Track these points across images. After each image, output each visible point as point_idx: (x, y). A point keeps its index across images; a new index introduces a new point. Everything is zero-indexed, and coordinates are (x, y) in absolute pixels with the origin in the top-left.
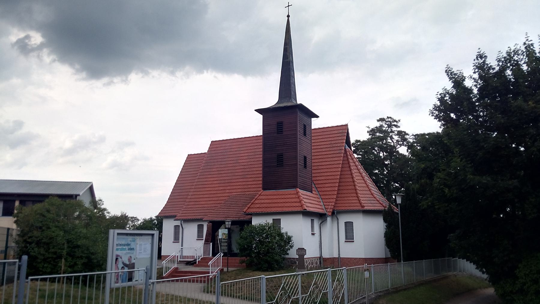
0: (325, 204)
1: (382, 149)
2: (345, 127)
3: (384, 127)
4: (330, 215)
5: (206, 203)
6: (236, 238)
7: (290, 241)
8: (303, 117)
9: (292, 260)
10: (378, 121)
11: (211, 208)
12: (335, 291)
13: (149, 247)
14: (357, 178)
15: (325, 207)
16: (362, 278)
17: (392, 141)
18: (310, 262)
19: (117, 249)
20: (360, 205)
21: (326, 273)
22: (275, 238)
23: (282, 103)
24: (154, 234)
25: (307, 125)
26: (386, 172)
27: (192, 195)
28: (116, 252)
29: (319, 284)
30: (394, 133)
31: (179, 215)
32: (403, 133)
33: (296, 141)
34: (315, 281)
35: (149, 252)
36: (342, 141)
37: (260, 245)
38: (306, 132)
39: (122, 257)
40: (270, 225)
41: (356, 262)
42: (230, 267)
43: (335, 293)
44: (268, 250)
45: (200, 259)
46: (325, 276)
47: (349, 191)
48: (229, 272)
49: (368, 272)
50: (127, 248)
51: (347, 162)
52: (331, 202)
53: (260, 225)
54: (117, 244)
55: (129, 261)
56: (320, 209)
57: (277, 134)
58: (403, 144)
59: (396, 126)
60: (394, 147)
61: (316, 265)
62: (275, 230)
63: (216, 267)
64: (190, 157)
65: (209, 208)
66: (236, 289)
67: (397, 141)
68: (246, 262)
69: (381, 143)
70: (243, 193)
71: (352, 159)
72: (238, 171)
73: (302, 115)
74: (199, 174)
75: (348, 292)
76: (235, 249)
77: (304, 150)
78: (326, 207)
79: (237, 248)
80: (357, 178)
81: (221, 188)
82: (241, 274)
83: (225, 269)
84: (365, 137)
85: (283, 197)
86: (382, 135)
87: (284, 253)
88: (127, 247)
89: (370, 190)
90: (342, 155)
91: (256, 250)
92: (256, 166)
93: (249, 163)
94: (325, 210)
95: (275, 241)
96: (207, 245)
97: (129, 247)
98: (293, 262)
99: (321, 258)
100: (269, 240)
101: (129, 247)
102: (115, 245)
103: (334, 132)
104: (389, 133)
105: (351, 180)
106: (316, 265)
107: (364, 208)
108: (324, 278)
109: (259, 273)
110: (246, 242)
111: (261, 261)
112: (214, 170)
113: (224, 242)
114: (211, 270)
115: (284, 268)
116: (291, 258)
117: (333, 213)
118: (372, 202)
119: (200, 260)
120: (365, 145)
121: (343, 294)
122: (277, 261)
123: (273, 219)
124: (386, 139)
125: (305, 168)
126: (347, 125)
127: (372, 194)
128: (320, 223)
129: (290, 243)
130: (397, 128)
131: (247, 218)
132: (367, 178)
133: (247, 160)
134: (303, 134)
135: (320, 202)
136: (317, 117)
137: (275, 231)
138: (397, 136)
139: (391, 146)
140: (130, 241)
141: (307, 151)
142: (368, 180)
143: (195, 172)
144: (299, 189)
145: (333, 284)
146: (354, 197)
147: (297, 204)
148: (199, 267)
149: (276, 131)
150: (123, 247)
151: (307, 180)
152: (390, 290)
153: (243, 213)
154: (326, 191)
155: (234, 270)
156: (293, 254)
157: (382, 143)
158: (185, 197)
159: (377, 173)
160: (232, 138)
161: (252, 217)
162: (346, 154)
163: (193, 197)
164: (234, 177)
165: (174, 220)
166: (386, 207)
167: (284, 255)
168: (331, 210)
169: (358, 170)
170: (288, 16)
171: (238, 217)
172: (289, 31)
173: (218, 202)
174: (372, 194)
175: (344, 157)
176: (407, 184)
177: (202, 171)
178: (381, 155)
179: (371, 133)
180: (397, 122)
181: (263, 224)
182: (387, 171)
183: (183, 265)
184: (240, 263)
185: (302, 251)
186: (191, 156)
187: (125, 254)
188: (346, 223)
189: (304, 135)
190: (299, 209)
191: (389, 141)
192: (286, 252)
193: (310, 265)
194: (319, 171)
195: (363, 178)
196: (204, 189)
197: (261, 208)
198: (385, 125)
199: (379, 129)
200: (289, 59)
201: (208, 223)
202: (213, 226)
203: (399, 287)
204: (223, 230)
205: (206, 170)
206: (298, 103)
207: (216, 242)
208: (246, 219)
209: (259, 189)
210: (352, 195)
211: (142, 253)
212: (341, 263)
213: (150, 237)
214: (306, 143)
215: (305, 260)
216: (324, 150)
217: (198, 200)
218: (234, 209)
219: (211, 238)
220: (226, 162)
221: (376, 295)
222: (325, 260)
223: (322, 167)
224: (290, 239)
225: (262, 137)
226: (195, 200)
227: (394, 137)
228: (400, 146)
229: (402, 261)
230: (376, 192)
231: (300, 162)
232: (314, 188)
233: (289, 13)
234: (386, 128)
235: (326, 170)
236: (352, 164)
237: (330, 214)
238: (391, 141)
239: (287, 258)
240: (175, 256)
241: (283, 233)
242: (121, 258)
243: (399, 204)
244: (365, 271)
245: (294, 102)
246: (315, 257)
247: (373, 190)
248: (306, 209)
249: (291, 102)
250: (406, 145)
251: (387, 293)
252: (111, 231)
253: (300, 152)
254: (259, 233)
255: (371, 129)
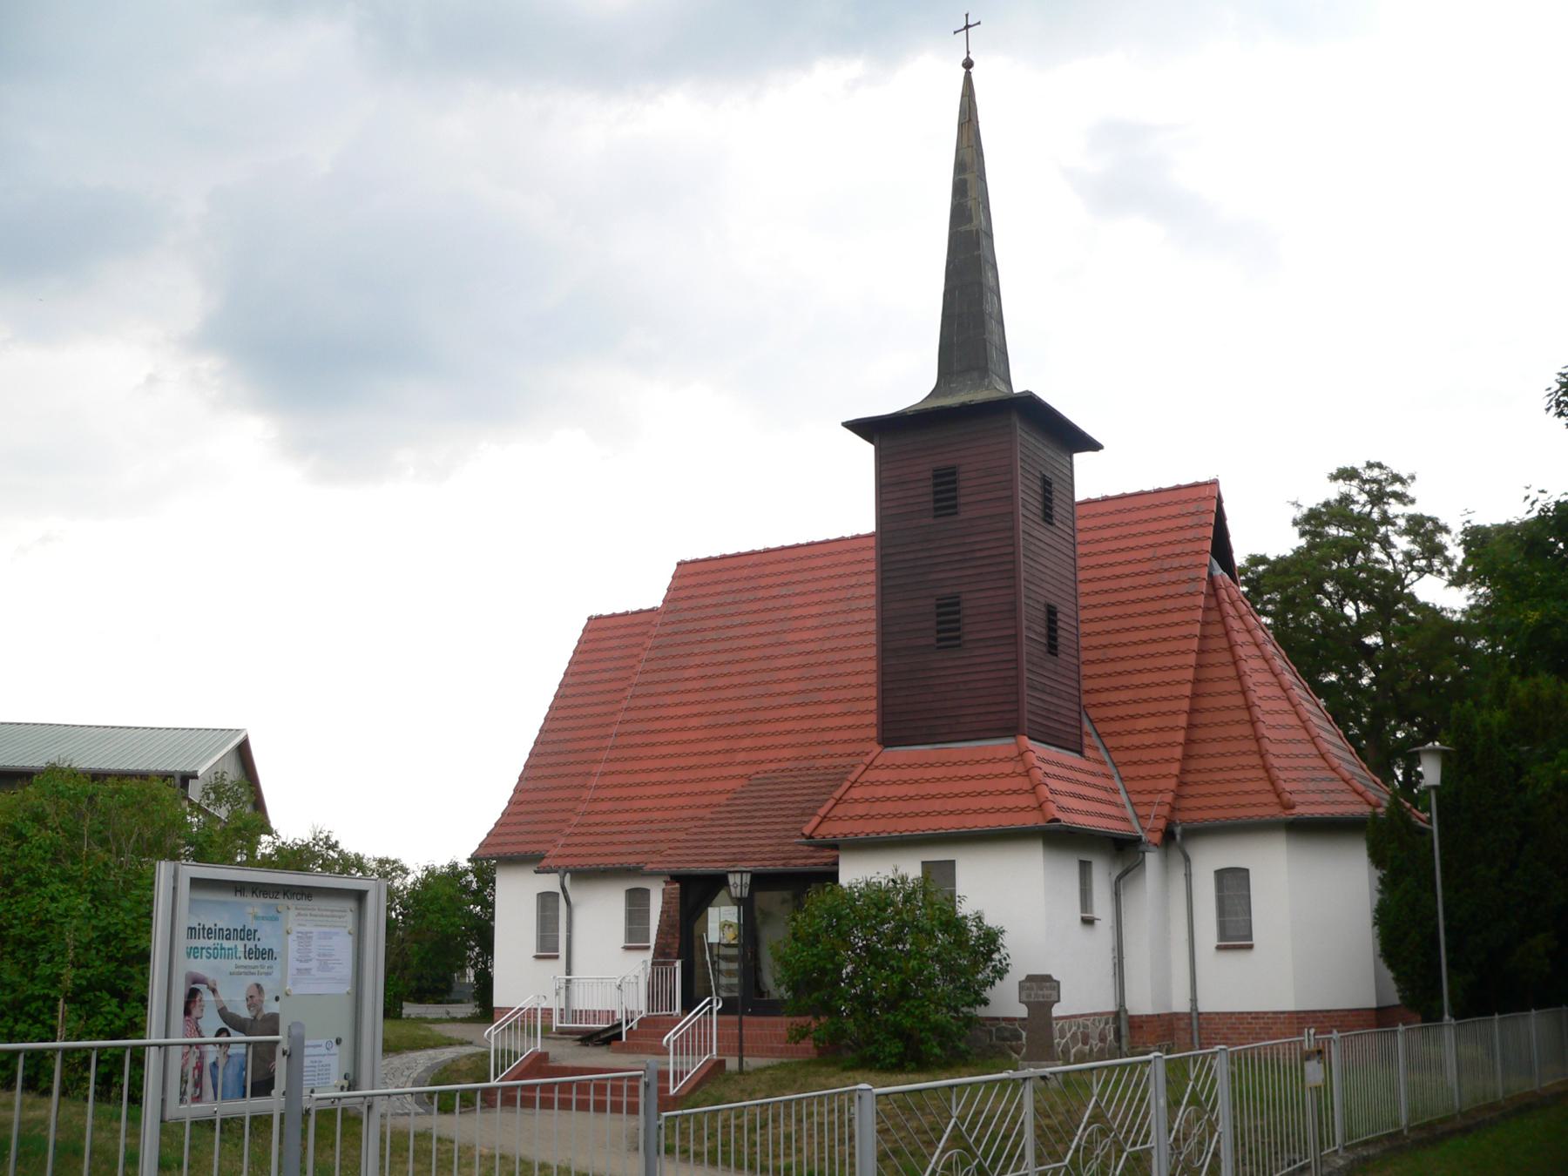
0: (1136, 798)
1: (1351, 587)
2: (1207, 492)
3: (1357, 502)
4: (1156, 845)
5: (658, 803)
6: (775, 937)
7: (993, 952)
8: (1040, 446)
9: (1003, 1024)
10: (1334, 478)
11: (679, 825)
12: (1178, 1147)
13: (342, 946)
14: (1261, 692)
15: (1135, 812)
16: (1297, 1092)
17: (1390, 556)
18: (1074, 1035)
19: (193, 952)
20: (1276, 800)
21: (1142, 1073)
22: (930, 935)
23: (951, 393)
24: (366, 892)
25: (1057, 480)
26: (1371, 679)
27: (604, 774)
28: (187, 966)
29: (1114, 1117)
30: (1394, 524)
31: (555, 852)
32: (1429, 525)
33: (1013, 545)
34: (1094, 1107)
35: (346, 969)
36: (1196, 547)
37: (872, 968)
38: (1051, 509)
39: (218, 989)
40: (909, 886)
41: (1261, 1028)
42: (748, 1056)
43: (1181, 1153)
44: (904, 984)
45: (634, 1024)
46: (1137, 1085)
47: (1233, 747)
48: (749, 1073)
49: (1319, 1063)
50: (241, 949)
51: (1218, 630)
52: (1161, 792)
53: (867, 884)
54: (191, 929)
55: (249, 1007)
56: (1116, 818)
57: (935, 517)
58: (1429, 569)
59: (1400, 497)
60: (1398, 578)
61: (1099, 1044)
62: (932, 904)
63: (693, 1054)
64: (598, 630)
65: (669, 826)
66: (776, 1143)
67: (1409, 557)
68: (816, 1034)
69: (1346, 564)
70: (805, 764)
71: (1241, 617)
72: (782, 675)
73: (1033, 441)
74: (629, 692)
75: (1236, 1145)
76: (773, 983)
77: (1048, 579)
78: (1142, 811)
79: (775, 980)
80: (1261, 692)
81: (718, 746)
82: (795, 1081)
83: (732, 1063)
84: (1283, 542)
85: (964, 771)
86: (1348, 534)
87: (969, 995)
88: (240, 945)
89: (1313, 740)
90: (1201, 600)
91: (854, 987)
92: (854, 655)
93: (827, 645)
94: (1135, 823)
95: (930, 950)
96: (664, 968)
97: (250, 944)
98: (1007, 1034)
99: (1122, 1015)
100: (908, 946)
101: (250, 944)
102: (181, 932)
103: (1164, 512)
104: (1374, 526)
105: (1239, 700)
106: (1099, 1044)
107: (1294, 811)
108: (1135, 1092)
109: (865, 1076)
110: (813, 955)
111: (875, 1031)
112: (687, 674)
113: (728, 959)
114: (675, 1063)
115: (969, 1058)
116: (997, 1019)
117: (1168, 837)
118: (1323, 786)
119: (635, 1028)
120: (1286, 571)
121: (1216, 1155)
122: (941, 1032)
123: (923, 863)
124: (1367, 550)
125: (1050, 652)
126: (1215, 483)
127: (1323, 756)
128: (1114, 878)
129: (994, 956)
130: (1405, 504)
131: (817, 861)
132: (1299, 692)
133: (820, 634)
134: (1042, 516)
135: (1116, 791)
136: (1094, 446)
137: (932, 907)
138: (1406, 538)
139: (1386, 572)
140: (256, 917)
141: (1058, 584)
142: (1307, 701)
143: (614, 686)
144: (1030, 738)
145: (1171, 1121)
146: (1253, 767)
147: (1023, 801)
148: (629, 1053)
149: (931, 505)
150: (220, 942)
151: (1061, 703)
152: (1405, 1132)
153: (804, 840)
154: (1138, 747)
155: (769, 1067)
156: (1005, 1001)
157: (1352, 562)
158: (577, 781)
159: (1332, 682)
160: (759, 547)
161: (838, 856)
162: (1217, 600)
163: (608, 780)
164: (766, 702)
165: (536, 872)
166: (1379, 806)
167: (969, 1005)
168: (1161, 824)
169: (1267, 661)
170: (968, 64)
171: (784, 859)
172: (970, 120)
173: (706, 800)
174: (1323, 756)
175: (1207, 609)
176: (1461, 707)
177: (643, 678)
178: (1349, 610)
179: (1307, 527)
180: (1403, 482)
181: (884, 882)
182: (1372, 675)
183: (570, 1043)
184: (791, 1038)
185: (1041, 988)
186: (600, 623)
187: (231, 974)
188: (1221, 875)
189: (1046, 521)
190: (1032, 820)
191: (1378, 554)
192: (977, 994)
193: (1075, 1044)
194: (1110, 668)
195: (1285, 691)
196: (648, 751)
197: (873, 817)
198: (1359, 494)
199: (1338, 511)
200: (975, 222)
201: (666, 882)
202: (684, 893)
203: (1441, 1121)
204: (723, 908)
205: (656, 677)
206: (1018, 387)
207: (697, 958)
208: (816, 864)
209: (867, 746)
210: (1243, 760)
211: (314, 972)
212: (1199, 1033)
213: (350, 905)
214: (1054, 552)
215: (1056, 1027)
216: (1126, 583)
217: (624, 792)
218: (769, 827)
219: (677, 940)
220: (735, 644)
221: (1351, 1157)
222: (1137, 1023)
223: (1121, 652)
224: (994, 941)
225: (874, 538)
226: (617, 793)
227: (1394, 539)
228: (1420, 577)
229: (1447, 1017)
230: (1334, 745)
231: (1031, 630)
232: (1089, 735)
233: (968, 53)
234: (1364, 505)
235: (1140, 664)
236: (1240, 638)
237: (1157, 837)
238: (1382, 557)
239: (982, 1018)
240: (536, 1009)
241: (966, 917)
242: (214, 991)
243: (1435, 787)
244: (1307, 1057)
245: (1003, 388)
246: (1095, 1014)
247: (1325, 740)
248: (1058, 820)
249: (987, 389)
250: (1440, 573)
251: (1395, 1144)
252: (164, 869)
253: (1031, 587)
254: (867, 917)
255: (1305, 511)
